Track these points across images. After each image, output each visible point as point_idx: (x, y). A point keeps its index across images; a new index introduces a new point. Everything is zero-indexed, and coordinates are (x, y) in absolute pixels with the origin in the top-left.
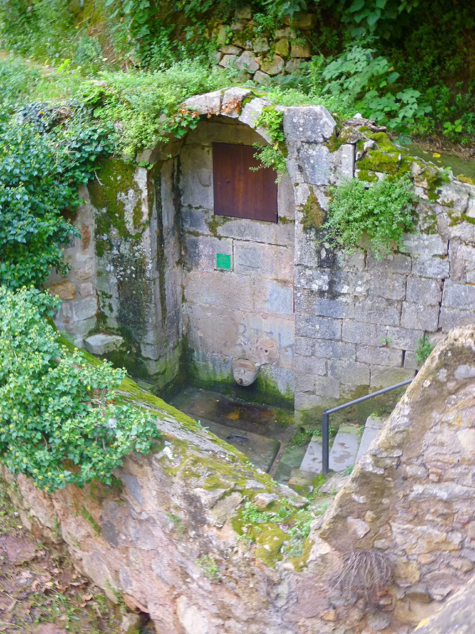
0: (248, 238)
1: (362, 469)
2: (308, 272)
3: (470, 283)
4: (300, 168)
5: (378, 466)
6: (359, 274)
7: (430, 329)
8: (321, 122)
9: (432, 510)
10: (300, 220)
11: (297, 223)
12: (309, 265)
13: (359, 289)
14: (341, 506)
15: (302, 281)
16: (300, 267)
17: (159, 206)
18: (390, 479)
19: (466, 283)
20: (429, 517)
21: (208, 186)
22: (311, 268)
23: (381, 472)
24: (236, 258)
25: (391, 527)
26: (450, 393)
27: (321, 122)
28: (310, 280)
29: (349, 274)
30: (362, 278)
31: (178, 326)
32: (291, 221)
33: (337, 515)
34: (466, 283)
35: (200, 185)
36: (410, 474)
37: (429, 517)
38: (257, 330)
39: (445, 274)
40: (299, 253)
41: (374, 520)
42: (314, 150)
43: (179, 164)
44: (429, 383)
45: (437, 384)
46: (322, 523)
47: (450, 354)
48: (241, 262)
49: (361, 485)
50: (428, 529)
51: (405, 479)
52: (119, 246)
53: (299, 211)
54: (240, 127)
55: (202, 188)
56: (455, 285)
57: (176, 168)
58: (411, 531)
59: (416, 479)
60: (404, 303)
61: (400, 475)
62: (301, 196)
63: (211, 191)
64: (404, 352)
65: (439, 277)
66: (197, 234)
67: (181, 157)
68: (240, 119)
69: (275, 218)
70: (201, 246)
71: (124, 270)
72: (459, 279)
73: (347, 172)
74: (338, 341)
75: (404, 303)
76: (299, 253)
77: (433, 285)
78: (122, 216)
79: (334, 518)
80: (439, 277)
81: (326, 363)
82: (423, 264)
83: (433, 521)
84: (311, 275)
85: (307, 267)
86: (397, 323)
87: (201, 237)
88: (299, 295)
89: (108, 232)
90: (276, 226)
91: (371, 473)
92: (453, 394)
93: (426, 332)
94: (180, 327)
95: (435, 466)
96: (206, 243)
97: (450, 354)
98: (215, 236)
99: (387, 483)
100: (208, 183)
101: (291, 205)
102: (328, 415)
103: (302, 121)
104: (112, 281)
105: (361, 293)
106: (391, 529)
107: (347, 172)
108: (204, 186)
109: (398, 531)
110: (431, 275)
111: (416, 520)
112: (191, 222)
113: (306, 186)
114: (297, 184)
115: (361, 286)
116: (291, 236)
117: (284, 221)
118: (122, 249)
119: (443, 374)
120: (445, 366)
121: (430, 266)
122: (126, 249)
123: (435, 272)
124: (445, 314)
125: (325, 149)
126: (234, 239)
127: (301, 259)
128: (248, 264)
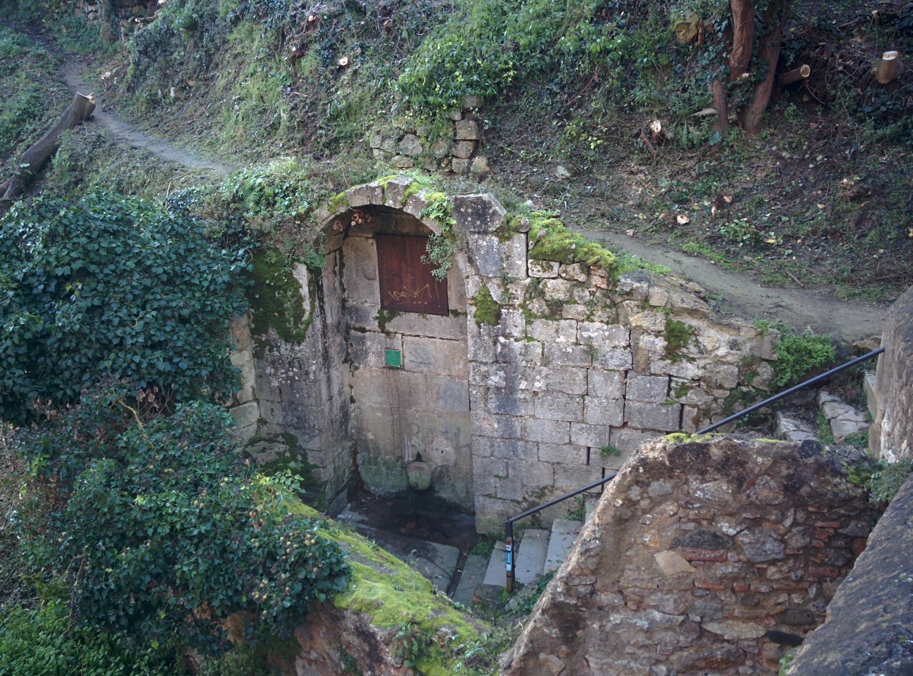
0: (418, 333)
1: (553, 599)
2: (483, 368)
3: (654, 374)
4: (471, 260)
5: (570, 595)
6: (537, 368)
7: (616, 425)
8: (491, 211)
9: (632, 642)
10: (473, 313)
11: (469, 317)
12: (484, 361)
13: (537, 384)
14: (531, 642)
15: (477, 378)
16: (474, 364)
17: (321, 300)
18: (584, 609)
19: (651, 375)
20: (628, 650)
21: (373, 279)
22: (486, 364)
23: (574, 602)
24: (407, 354)
25: (587, 661)
26: (645, 512)
27: (491, 211)
28: (485, 376)
29: (527, 369)
30: (540, 373)
31: (346, 429)
32: (463, 314)
33: (528, 652)
34: (651, 375)
35: (364, 279)
36: (605, 602)
37: (628, 650)
38: (431, 430)
39: (628, 366)
40: (472, 348)
41: (568, 655)
42: (484, 240)
43: (341, 258)
44: (620, 502)
45: (630, 503)
46: (512, 661)
47: (641, 470)
48: (412, 358)
49: (553, 617)
50: (629, 663)
51: (600, 608)
52: (279, 347)
53: (471, 305)
54: (403, 217)
55: (367, 281)
56: (639, 377)
57: (338, 261)
58: (610, 665)
59: (614, 608)
60: (586, 397)
61: (594, 604)
62: (471, 289)
63: (377, 284)
64: (589, 448)
65: (622, 369)
66: (363, 330)
67: (343, 249)
68: (405, 210)
69: (444, 310)
70: (369, 343)
71: (286, 373)
72: (644, 370)
73: (519, 262)
74: (519, 439)
75: (586, 397)
76: (472, 348)
77: (616, 377)
78: (282, 314)
79: (525, 655)
80: (622, 369)
81: (507, 463)
82: (604, 356)
83: (634, 654)
84: (487, 371)
85: (481, 363)
86: (580, 418)
87: (367, 334)
88: (474, 392)
89: (266, 332)
90: (448, 319)
91: (563, 602)
92: (648, 513)
93: (611, 427)
94: (349, 430)
95: (633, 593)
96: (373, 340)
97: (641, 470)
98: (383, 332)
99: (581, 613)
100: (373, 277)
101: (462, 296)
102: (511, 522)
103: (470, 210)
104: (273, 384)
105: (540, 388)
106: (589, 665)
107: (519, 262)
108: (369, 279)
109: (596, 667)
110: (613, 368)
111: (615, 653)
112: (357, 319)
113: (477, 278)
114: (467, 277)
115: (539, 381)
116: (463, 329)
117: (456, 313)
118: (282, 350)
119: (635, 493)
120: (637, 483)
121: (612, 357)
122: (286, 349)
123: (617, 363)
124: (630, 408)
125: (495, 240)
126: (403, 335)
127: (476, 354)
128: (420, 360)
